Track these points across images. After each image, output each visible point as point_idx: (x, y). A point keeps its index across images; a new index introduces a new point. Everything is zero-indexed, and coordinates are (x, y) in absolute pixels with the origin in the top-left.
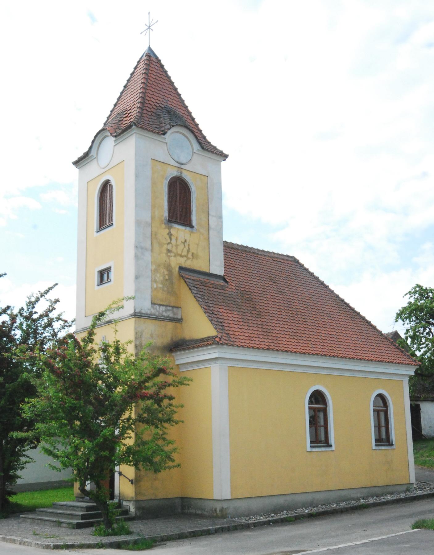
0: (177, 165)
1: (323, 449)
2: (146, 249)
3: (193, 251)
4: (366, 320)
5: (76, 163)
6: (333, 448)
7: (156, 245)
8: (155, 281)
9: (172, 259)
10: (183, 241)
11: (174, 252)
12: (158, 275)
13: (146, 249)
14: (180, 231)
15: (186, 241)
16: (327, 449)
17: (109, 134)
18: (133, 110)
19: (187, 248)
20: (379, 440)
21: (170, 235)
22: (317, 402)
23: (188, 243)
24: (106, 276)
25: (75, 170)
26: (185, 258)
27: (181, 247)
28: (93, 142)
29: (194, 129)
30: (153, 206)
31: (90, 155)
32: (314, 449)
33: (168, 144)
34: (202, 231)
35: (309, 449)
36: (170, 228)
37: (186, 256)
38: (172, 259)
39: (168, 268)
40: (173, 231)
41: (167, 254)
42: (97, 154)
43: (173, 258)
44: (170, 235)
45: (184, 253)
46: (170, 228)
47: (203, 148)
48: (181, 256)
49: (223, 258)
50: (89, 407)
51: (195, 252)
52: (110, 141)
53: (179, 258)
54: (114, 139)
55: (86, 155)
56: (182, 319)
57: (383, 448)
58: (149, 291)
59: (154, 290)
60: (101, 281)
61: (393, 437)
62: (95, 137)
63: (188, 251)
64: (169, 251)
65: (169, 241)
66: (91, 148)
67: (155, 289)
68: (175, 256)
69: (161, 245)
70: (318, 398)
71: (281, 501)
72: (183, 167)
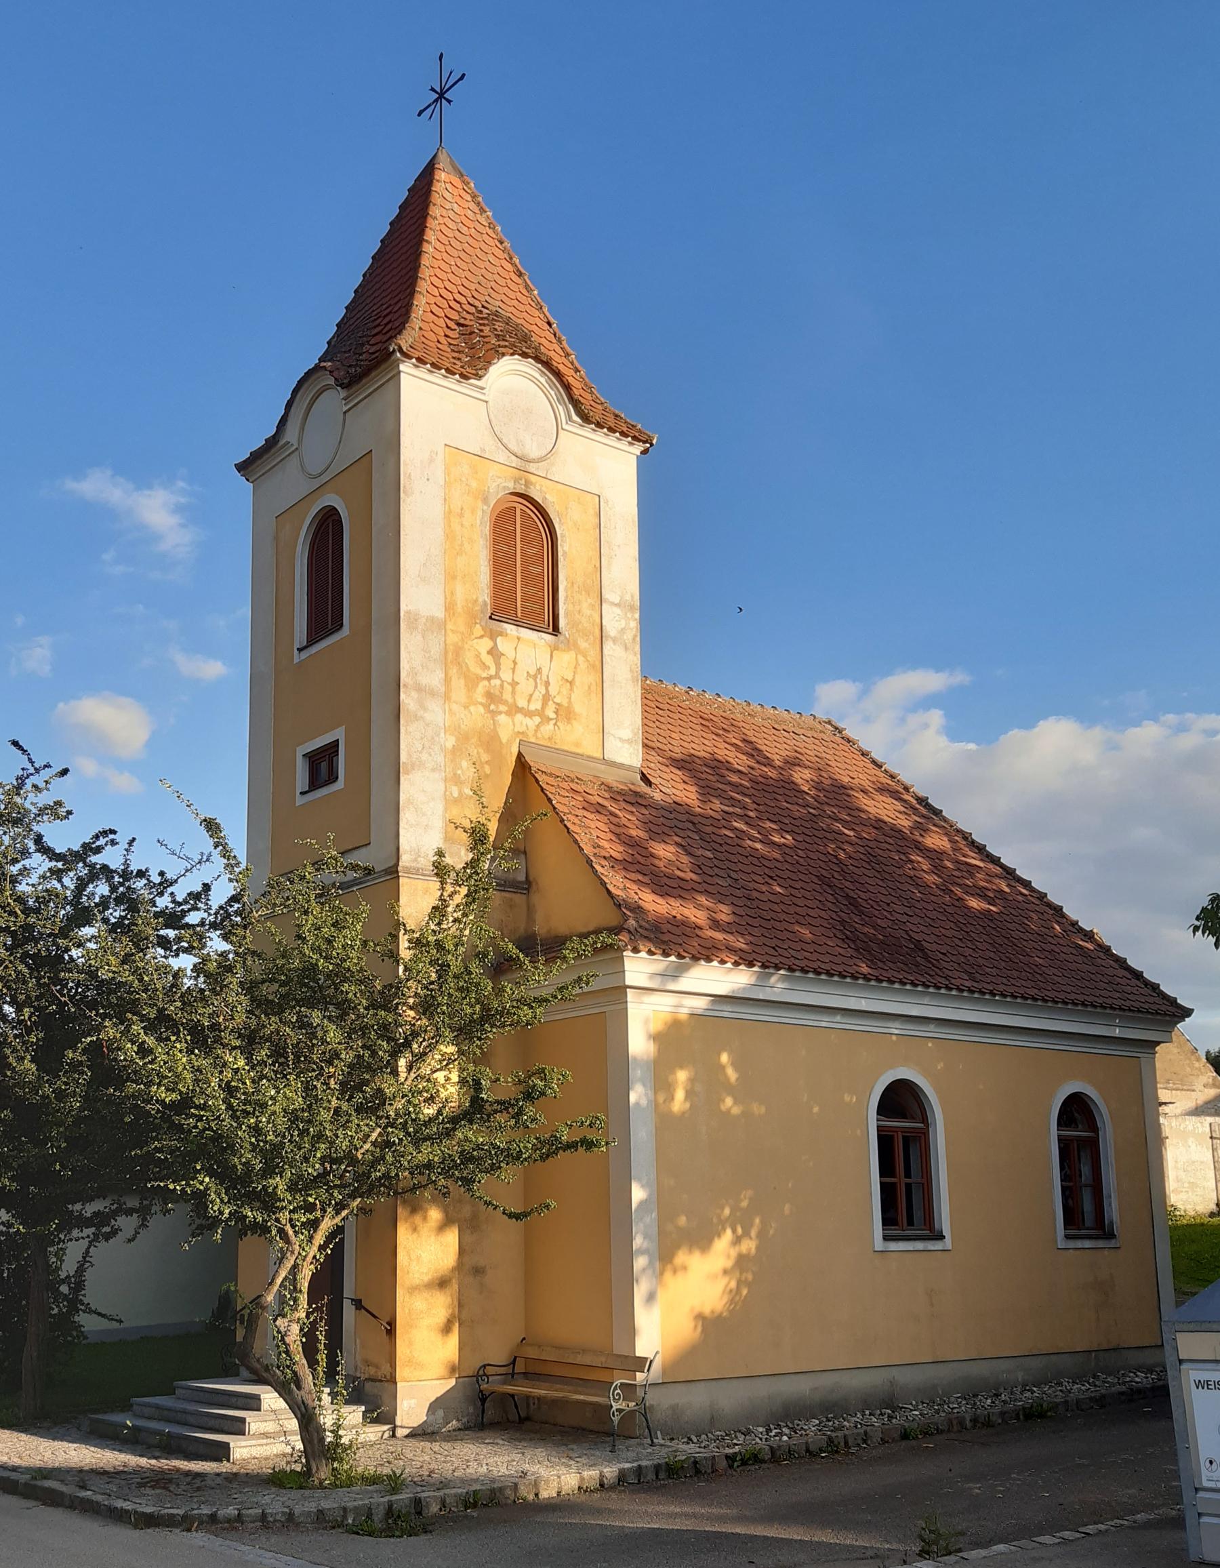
0: (515, 462)
1: (919, 1245)
2: (432, 693)
3: (558, 700)
4: (1082, 929)
5: (242, 467)
6: (948, 1243)
7: (458, 684)
8: (456, 780)
9: (502, 719)
10: (532, 672)
11: (505, 703)
12: (464, 764)
13: (432, 693)
14: (525, 647)
15: (539, 670)
16: (931, 1245)
17: (332, 381)
18: (397, 315)
19: (544, 691)
20: (1072, 1217)
21: (494, 652)
22: (902, 1114)
23: (544, 678)
24: (324, 765)
25: (245, 487)
26: (537, 719)
27: (525, 686)
28: (289, 405)
29: (561, 367)
30: (451, 577)
31: (281, 443)
32: (893, 1246)
33: (490, 403)
34: (583, 644)
35: (879, 1244)
36: (493, 636)
37: (541, 713)
38: (502, 719)
39: (490, 741)
40: (503, 645)
41: (486, 707)
42: (300, 441)
43: (503, 716)
44: (494, 652)
45: (536, 705)
46: (493, 636)
47: (586, 419)
48: (529, 714)
49: (639, 722)
50: (328, 1440)
51: (565, 703)
52: (333, 400)
53: (519, 717)
54: (343, 393)
55: (272, 443)
56: (528, 881)
57: (1087, 1244)
58: (439, 807)
59: (450, 802)
60: (315, 783)
61: (1114, 1210)
62: (295, 392)
63: (546, 698)
64: (490, 696)
65: (493, 671)
66: (283, 421)
67: (456, 801)
68: (508, 713)
69: (472, 682)
70: (901, 1101)
71: (802, 1388)
72: (532, 468)
